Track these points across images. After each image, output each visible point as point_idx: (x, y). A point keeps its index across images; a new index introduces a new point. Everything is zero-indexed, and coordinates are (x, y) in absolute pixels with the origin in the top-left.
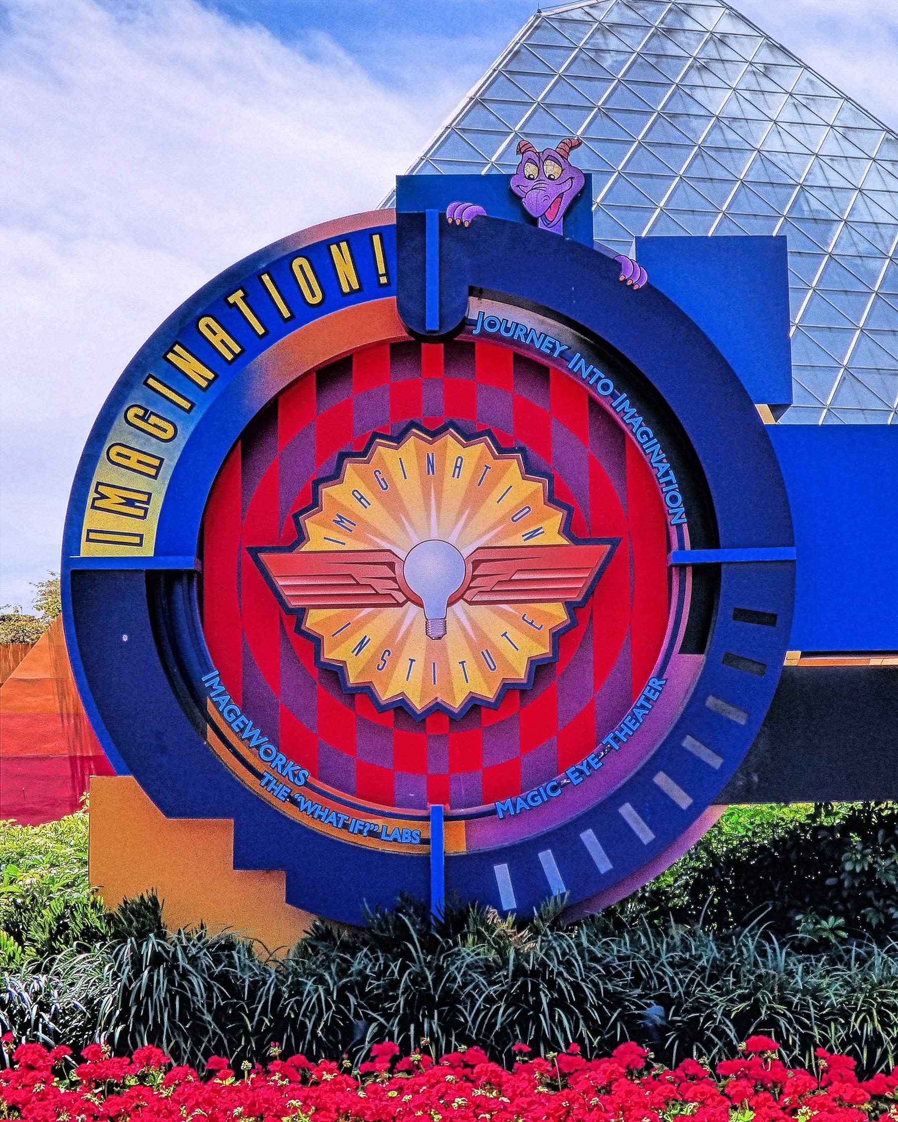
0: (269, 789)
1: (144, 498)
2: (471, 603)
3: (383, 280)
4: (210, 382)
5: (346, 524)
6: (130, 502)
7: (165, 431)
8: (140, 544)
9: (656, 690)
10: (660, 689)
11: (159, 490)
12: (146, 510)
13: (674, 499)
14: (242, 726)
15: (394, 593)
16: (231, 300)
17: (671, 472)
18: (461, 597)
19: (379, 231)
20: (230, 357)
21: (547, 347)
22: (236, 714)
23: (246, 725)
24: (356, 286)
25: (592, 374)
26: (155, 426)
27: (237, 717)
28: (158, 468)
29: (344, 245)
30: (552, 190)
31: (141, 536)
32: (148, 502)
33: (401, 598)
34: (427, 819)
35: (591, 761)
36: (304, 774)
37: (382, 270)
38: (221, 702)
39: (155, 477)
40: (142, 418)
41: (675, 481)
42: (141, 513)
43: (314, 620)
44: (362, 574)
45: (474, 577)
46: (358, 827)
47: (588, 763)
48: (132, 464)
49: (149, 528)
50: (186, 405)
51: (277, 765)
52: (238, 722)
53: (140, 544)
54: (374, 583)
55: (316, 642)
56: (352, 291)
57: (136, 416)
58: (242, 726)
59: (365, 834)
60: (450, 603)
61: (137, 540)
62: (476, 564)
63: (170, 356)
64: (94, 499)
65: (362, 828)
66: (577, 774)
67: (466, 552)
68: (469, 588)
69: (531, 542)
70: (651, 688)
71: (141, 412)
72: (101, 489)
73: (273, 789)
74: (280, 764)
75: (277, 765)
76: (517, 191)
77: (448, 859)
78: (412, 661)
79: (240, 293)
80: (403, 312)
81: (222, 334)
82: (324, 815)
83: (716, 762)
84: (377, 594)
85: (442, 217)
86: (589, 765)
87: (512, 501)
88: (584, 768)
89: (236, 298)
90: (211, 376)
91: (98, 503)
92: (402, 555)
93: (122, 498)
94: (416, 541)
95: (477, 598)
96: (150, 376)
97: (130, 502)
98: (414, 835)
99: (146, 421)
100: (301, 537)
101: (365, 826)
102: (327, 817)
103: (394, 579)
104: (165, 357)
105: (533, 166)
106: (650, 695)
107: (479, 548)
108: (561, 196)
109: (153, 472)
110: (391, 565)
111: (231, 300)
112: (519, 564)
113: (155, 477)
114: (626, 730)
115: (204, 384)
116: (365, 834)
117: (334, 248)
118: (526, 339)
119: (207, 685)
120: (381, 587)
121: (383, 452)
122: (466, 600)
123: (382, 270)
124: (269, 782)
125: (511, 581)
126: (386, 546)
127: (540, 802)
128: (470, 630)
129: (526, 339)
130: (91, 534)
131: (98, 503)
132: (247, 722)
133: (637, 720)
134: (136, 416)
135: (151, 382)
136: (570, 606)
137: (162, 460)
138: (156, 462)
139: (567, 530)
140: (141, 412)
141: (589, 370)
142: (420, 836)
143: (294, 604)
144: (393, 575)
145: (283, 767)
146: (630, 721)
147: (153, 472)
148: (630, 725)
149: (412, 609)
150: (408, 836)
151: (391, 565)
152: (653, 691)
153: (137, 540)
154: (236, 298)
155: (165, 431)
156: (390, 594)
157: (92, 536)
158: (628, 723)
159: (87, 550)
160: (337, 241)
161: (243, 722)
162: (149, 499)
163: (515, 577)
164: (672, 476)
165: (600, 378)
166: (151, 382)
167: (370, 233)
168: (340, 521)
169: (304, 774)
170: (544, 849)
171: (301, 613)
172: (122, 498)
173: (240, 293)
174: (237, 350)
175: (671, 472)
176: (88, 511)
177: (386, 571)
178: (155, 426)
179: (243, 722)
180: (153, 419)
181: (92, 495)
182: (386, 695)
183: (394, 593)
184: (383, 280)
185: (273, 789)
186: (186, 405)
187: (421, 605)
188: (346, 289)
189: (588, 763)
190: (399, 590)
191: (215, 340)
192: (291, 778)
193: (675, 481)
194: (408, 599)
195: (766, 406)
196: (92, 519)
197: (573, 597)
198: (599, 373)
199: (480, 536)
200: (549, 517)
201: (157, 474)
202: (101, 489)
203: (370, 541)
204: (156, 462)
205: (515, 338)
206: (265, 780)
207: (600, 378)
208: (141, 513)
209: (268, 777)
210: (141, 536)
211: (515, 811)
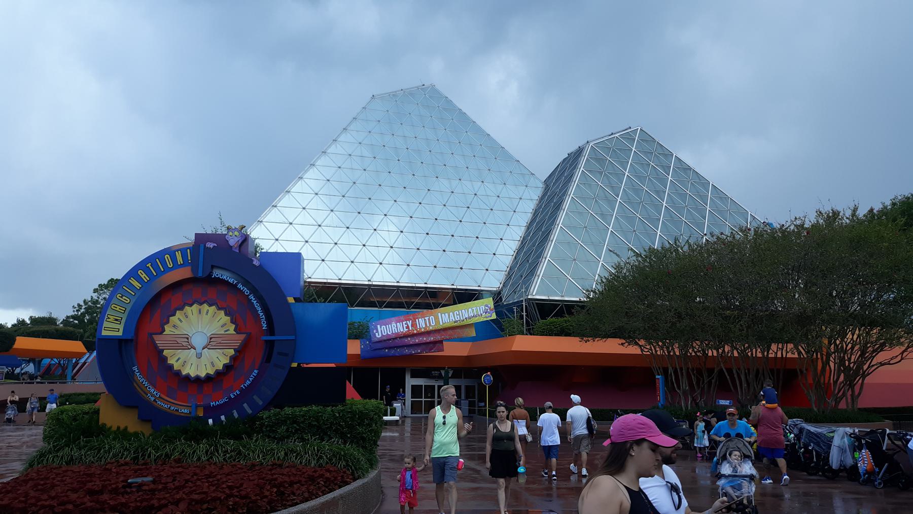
1: (121, 319)
6: (116, 320)
24: (182, 263)
28: (125, 311)
30: (237, 239)
37: (189, 259)
40: (121, 297)
42: (119, 323)
43: (166, 353)
44: (179, 340)
45: (210, 342)
48: (117, 309)
49: (121, 327)
50: (134, 294)
54: (183, 343)
55: (165, 359)
56: (181, 264)
60: (203, 349)
61: (118, 330)
62: (211, 338)
69: (226, 333)
71: (121, 296)
77: (519, 435)
78: (205, 365)
79: (150, 264)
80: (192, 270)
81: (144, 275)
83: (384, 397)
85: (205, 246)
86: (236, 393)
87: (221, 322)
88: (235, 393)
89: (149, 265)
90: (140, 286)
91: (107, 320)
94: (205, 332)
95: (211, 348)
97: (116, 320)
103: (188, 342)
108: (238, 241)
109: (123, 312)
110: (188, 338)
111: (147, 266)
112: (224, 339)
115: (139, 288)
117: (176, 252)
120: (184, 344)
123: (189, 259)
125: (220, 343)
128: (190, 355)
131: (107, 320)
135: (124, 287)
136: (235, 350)
137: (126, 309)
138: (124, 309)
140: (121, 296)
143: (160, 348)
144: (187, 341)
147: (123, 312)
151: (188, 338)
153: (118, 330)
154: (149, 265)
164: (264, 317)
166: (124, 287)
168: (174, 326)
171: (163, 350)
173: (150, 264)
174: (148, 279)
176: (105, 322)
177: (186, 340)
180: (124, 297)
181: (106, 317)
182: (184, 373)
184: (190, 261)
186: (134, 294)
188: (179, 263)
191: (142, 276)
199: (213, 330)
200: (231, 326)
203: (183, 332)
204: (124, 309)
208: (119, 323)
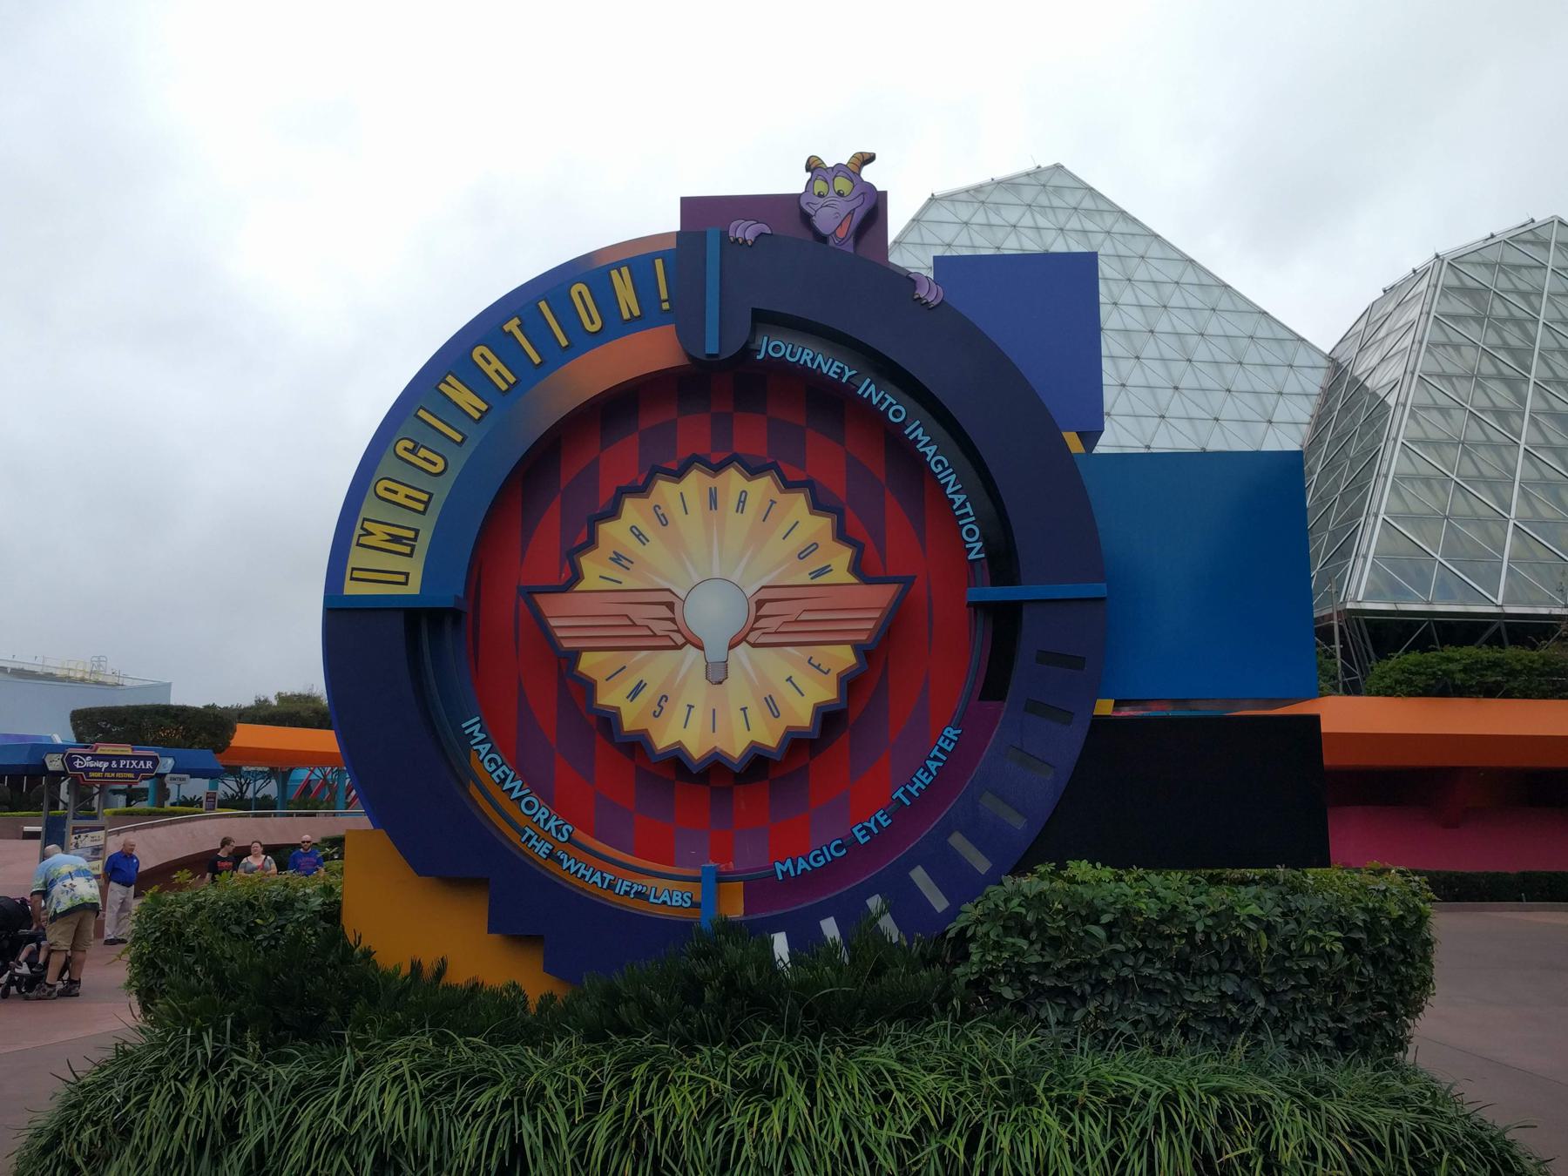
0: (530, 845)
1: (411, 534)
2: (754, 645)
3: (666, 306)
4: (484, 414)
5: (624, 562)
6: (396, 539)
7: (435, 464)
8: (406, 583)
9: (951, 740)
10: (956, 739)
11: (427, 528)
12: (413, 548)
13: (971, 533)
14: (503, 776)
15: (672, 634)
16: (507, 328)
17: (968, 504)
18: (744, 639)
19: (662, 255)
20: (504, 387)
21: (835, 372)
22: (496, 763)
23: (507, 776)
24: (637, 312)
25: (883, 399)
26: (425, 459)
27: (498, 767)
28: (427, 503)
29: (625, 270)
31: (407, 575)
32: (415, 539)
33: (679, 640)
34: (697, 880)
35: (879, 818)
36: (567, 830)
37: (664, 295)
38: (956, 500)
39: (423, 513)
40: (413, 451)
41: (972, 514)
42: (407, 550)
43: (589, 664)
44: (639, 614)
45: (758, 618)
46: (624, 888)
47: (876, 820)
48: (400, 498)
49: (415, 568)
50: (458, 438)
51: (539, 820)
52: (499, 772)
53: (406, 583)
56: (633, 318)
57: (406, 449)
58: (503, 776)
59: (632, 896)
60: (731, 647)
61: (402, 578)
63: (443, 387)
64: (360, 536)
65: (628, 889)
66: (864, 832)
67: (750, 591)
68: (752, 629)
70: (946, 738)
71: (410, 445)
72: (367, 525)
73: (533, 846)
74: (543, 818)
75: (539, 820)
76: (808, 209)
78: (690, 707)
79: (516, 321)
81: (497, 364)
82: (588, 874)
84: (655, 635)
87: (799, 539)
88: (872, 825)
89: (512, 326)
90: (484, 407)
91: (363, 540)
92: (682, 595)
93: (388, 534)
95: (760, 641)
96: (421, 408)
97: (396, 539)
98: (685, 897)
99: (416, 455)
100: (577, 576)
101: (632, 888)
102: (591, 877)
103: (673, 620)
104: (437, 388)
105: (823, 183)
106: (945, 746)
107: (763, 587)
109: (420, 507)
113: (423, 513)
114: (918, 784)
115: (476, 415)
116: (632, 896)
117: (614, 273)
118: (813, 364)
119: (467, 732)
120: (660, 627)
121: (798, 503)
122: (748, 642)
123: (664, 295)
124: (530, 838)
126: (666, 586)
127: (937, 471)
129: (813, 364)
130: (355, 572)
131: (365, 540)
132: (508, 771)
133: (931, 773)
134: (406, 449)
135: (422, 413)
136: (857, 648)
137: (431, 495)
138: (425, 497)
139: (856, 568)
140: (410, 445)
141: (880, 395)
142: (691, 899)
143: (567, 644)
145: (546, 821)
146: (922, 774)
147: (420, 507)
148: (923, 778)
149: (690, 651)
150: (679, 898)
152: (948, 741)
153: (402, 578)
155: (435, 464)
156: (668, 636)
157: (357, 574)
158: (920, 777)
159: (351, 588)
160: (618, 266)
161: (503, 772)
162: (416, 536)
163: (802, 617)
165: (891, 404)
166: (422, 413)
167: (652, 257)
169: (567, 830)
170: (826, 916)
171: (575, 655)
172: (388, 534)
173: (516, 321)
174: (512, 379)
175: (968, 504)
177: (664, 612)
178: (425, 459)
179: (503, 772)
180: (423, 453)
181: (358, 531)
183: (672, 634)
185: (533, 846)
186: (458, 438)
187: (701, 648)
188: (626, 315)
189: (876, 820)
190: (678, 631)
192: (554, 834)
193: (972, 514)
194: (688, 642)
195: (1074, 434)
196: (357, 557)
197: (863, 637)
198: (890, 399)
201: (426, 509)
202: (367, 525)
204: (425, 497)
205: (802, 362)
206: (526, 835)
207: (891, 404)
208: (407, 550)
209: (529, 832)
210: (407, 575)
211: (796, 872)
